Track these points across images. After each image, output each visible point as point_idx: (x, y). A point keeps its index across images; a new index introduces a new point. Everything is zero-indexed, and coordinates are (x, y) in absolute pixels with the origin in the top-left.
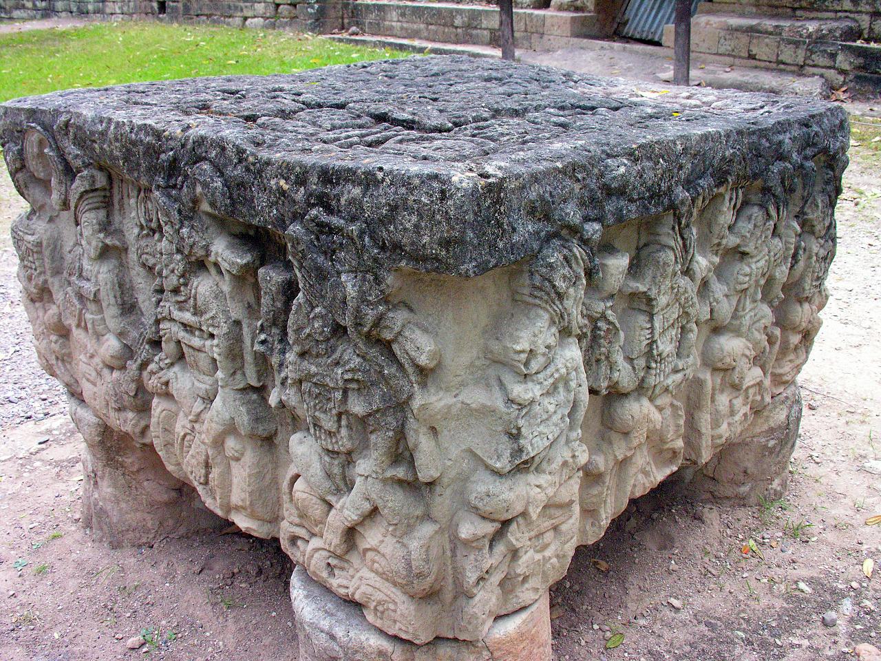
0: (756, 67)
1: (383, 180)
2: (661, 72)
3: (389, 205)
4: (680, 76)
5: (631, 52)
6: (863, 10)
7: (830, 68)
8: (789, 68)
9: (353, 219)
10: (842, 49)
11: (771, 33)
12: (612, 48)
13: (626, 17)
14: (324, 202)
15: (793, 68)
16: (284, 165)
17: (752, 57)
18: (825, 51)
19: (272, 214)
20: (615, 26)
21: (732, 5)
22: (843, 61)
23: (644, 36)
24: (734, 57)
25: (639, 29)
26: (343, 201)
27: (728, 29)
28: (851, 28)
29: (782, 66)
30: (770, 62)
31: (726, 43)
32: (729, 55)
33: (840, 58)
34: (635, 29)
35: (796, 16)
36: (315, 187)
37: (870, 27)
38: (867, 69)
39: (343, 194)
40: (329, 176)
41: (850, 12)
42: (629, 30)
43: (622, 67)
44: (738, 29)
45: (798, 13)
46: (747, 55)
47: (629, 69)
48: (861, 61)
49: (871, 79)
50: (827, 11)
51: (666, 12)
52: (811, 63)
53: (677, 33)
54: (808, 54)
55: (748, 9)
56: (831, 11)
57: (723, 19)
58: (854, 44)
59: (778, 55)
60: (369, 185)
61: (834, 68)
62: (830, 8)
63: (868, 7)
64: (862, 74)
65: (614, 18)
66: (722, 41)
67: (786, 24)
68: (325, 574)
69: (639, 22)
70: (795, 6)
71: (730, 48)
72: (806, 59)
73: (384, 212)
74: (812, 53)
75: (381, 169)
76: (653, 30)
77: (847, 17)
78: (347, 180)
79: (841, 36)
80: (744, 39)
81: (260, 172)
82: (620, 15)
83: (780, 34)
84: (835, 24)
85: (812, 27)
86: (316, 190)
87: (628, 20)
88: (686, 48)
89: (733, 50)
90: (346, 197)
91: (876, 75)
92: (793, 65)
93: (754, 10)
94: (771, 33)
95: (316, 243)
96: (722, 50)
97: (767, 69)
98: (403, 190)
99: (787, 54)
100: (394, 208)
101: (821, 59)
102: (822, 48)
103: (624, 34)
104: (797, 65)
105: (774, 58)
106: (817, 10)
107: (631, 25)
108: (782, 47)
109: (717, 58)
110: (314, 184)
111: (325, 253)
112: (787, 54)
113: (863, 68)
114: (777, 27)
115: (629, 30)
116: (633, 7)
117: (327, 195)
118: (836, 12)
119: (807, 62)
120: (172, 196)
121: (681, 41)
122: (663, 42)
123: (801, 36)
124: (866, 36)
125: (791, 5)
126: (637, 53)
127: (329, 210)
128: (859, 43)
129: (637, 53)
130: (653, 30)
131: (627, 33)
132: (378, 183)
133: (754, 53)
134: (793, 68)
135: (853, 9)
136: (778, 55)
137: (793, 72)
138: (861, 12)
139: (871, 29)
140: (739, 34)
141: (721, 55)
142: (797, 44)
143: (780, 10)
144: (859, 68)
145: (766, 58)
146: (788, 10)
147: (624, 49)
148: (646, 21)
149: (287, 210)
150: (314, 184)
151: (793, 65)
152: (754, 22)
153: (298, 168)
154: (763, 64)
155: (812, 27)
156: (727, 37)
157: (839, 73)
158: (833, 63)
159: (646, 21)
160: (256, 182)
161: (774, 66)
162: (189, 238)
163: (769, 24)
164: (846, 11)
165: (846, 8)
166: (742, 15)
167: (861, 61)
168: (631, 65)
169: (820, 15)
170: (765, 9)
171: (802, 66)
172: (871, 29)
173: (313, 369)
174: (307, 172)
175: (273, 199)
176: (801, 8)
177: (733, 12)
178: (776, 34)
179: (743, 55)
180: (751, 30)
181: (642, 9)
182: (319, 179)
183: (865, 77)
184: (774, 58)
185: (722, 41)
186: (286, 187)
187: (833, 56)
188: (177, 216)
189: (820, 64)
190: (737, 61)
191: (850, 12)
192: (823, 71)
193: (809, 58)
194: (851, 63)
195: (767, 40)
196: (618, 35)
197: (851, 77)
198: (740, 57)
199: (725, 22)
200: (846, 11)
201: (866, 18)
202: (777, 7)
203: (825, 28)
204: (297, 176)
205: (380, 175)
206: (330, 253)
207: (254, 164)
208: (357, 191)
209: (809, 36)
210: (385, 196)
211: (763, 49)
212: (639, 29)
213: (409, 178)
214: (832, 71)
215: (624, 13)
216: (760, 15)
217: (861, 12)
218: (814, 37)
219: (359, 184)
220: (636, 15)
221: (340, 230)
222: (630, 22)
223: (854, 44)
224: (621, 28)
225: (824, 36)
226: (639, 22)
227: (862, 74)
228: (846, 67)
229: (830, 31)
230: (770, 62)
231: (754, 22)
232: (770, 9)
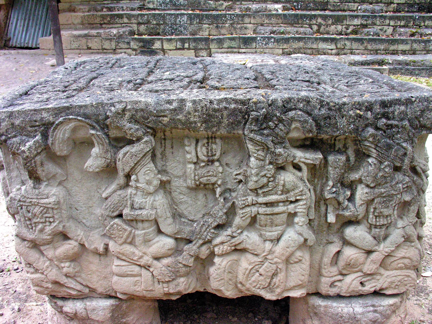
0: (92, 53)
1: (415, 101)
2: (46, 62)
3: (421, 110)
4: (60, 62)
5: (23, 54)
6: (133, 22)
7: (128, 49)
8: (109, 51)
9: (402, 120)
10: (132, 40)
11: (96, 36)
12: (11, 54)
13: (9, 36)
14: (385, 116)
15: (110, 51)
16: (356, 103)
17: (89, 48)
18: (124, 41)
19: (350, 128)
20: (4, 42)
21: (69, 25)
22: (133, 44)
23: (22, 45)
24: (80, 49)
25: (18, 42)
26: (396, 113)
27: (74, 37)
28: (131, 30)
29: (105, 51)
30: (99, 50)
31: (75, 43)
32: (77, 49)
33: (132, 43)
34: (16, 42)
35: (103, 28)
36: (379, 110)
37: (138, 29)
38: (145, 47)
39: (396, 110)
40: (384, 104)
41: (128, 23)
42: (13, 43)
43: (23, 62)
44: (80, 36)
45: (104, 26)
46: (86, 48)
47: (28, 63)
48: (142, 44)
49: (148, 51)
50: (117, 24)
51: (31, 32)
52: (119, 47)
53: (55, 41)
54: (117, 44)
55: (78, 26)
56: (119, 24)
57: (70, 32)
58: (142, 37)
59: (102, 46)
60: (407, 104)
61: (130, 48)
62: (118, 22)
63: (135, 21)
64: (143, 49)
65: (2, 38)
66: (72, 42)
67: (101, 31)
68: (360, 288)
69: (17, 38)
70: (102, 23)
71: (77, 46)
72: (116, 46)
73: (418, 113)
74: (118, 43)
75: (412, 97)
76: (26, 42)
77: (127, 26)
78: (395, 104)
79: (128, 34)
80: (84, 41)
81: (340, 109)
82: (5, 36)
83: (101, 36)
84: (124, 29)
85: (115, 31)
86: (380, 111)
87: (10, 39)
88: (61, 48)
89: (79, 46)
90: (398, 111)
91: (149, 50)
92: (110, 49)
93: (81, 26)
94: (96, 36)
95: (384, 134)
96: (73, 47)
97: (98, 53)
98: (425, 103)
99: (107, 45)
100: (423, 111)
101: (124, 45)
102: (123, 40)
103: (10, 46)
104: (112, 49)
105: (100, 48)
106: (112, 24)
107: (13, 40)
108: (103, 42)
109: (71, 51)
110: (377, 109)
111: (389, 138)
112: (107, 45)
113: (144, 47)
114: (98, 33)
115: (13, 43)
116: (11, 31)
117: (387, 112)
118: (121, 24)
119: (117, 47)
120: (264, 134)
121: (57, 45)
122: (40, 46)
123: (111, 36)
124: (137, 33)
125: (99, 23)
126: (26, 54)
127: (388, 118)
128: (136, 36)
129: (26, 54)
130: (26, 42)
131: (12, 45)
132: (412, 103)
133: (90, 46)
134: (110, 51)
135: (129, 22)
136: (102, 46)
137: (111, 53)
138: (132, 23)
139: (138, 30)
140: (81, 39)
141: (73, 49)
142: (111, 40)
143: (95, 25)
144: (141, 47)
145: (96, 48)
146: (98, 25)
147: (18, 53)
148: (21, 38)
149: (362, 123)
150: (377, 109)
151: (110, 49)
152: (86, 32)
153: (366, 104)
154: (95, 51)
155: (115, 31)
156: (75, 40)
157: (133, 50)
158: (129, 47)
159: (21, 38)
160: (337, 115)
161: (101, 51)
162: (285, 153)
163: (94, 32)
164: (126, 23)
165: (126, 22)
166: (76, 29)
167: (142, 44)
168: (28, 60)
169: (114, 26)
170: (87, 25)
171: (115, 50)
172: (138, 30)
173: (383, 190)
174: (372, 104)
175: (351, 120)
176: (105, 23)
177: (71, 28)
178: (99, 36)
179: (85, 48)
180: (86, 36)
181: (17, 32)
182: (380, 106)
183: (145, 51)
184: (100, 48)
185: (72, 42)
186: (361, 113)
187: (129, 43)
188: (272, 144)
189: (123, 47)
190: (82, 51)
191: (128, 23)
192: (125, 50)
193: (118, 45)
194: (137, 45)
195: (96, 40)
196: (7, 46)
197: (139, 51)
198: (83, 49)
199: (71, 33)
200: (126, 23)
201: (135, 26)
202: (93, 24)
203: (121, 31)
204: (366, 107)
205: (413, 99)
206: (391, 137)
207: (334, 106)
208: (403, 108)
209: (115, 36)
210: (417, 108)
211: (94, 44)
212: (18, 42)
213: (427, 98)
214: (130, 50)
215: (7, 35)
216: (85, 28)
217: (132, 23)
218: (117, 36)
219: (403, 105)
220: (14, 35)
221: (397, 126)
222: (12, 38)
223: (142, 37)
224: (7, 43)
225: (121, 35)
226: (17, 38)
227: (143, 49)
228: (136, 47)
229: (124, 32)
230: (99, 50)
231: (86, 32)
232: (89, 26)
